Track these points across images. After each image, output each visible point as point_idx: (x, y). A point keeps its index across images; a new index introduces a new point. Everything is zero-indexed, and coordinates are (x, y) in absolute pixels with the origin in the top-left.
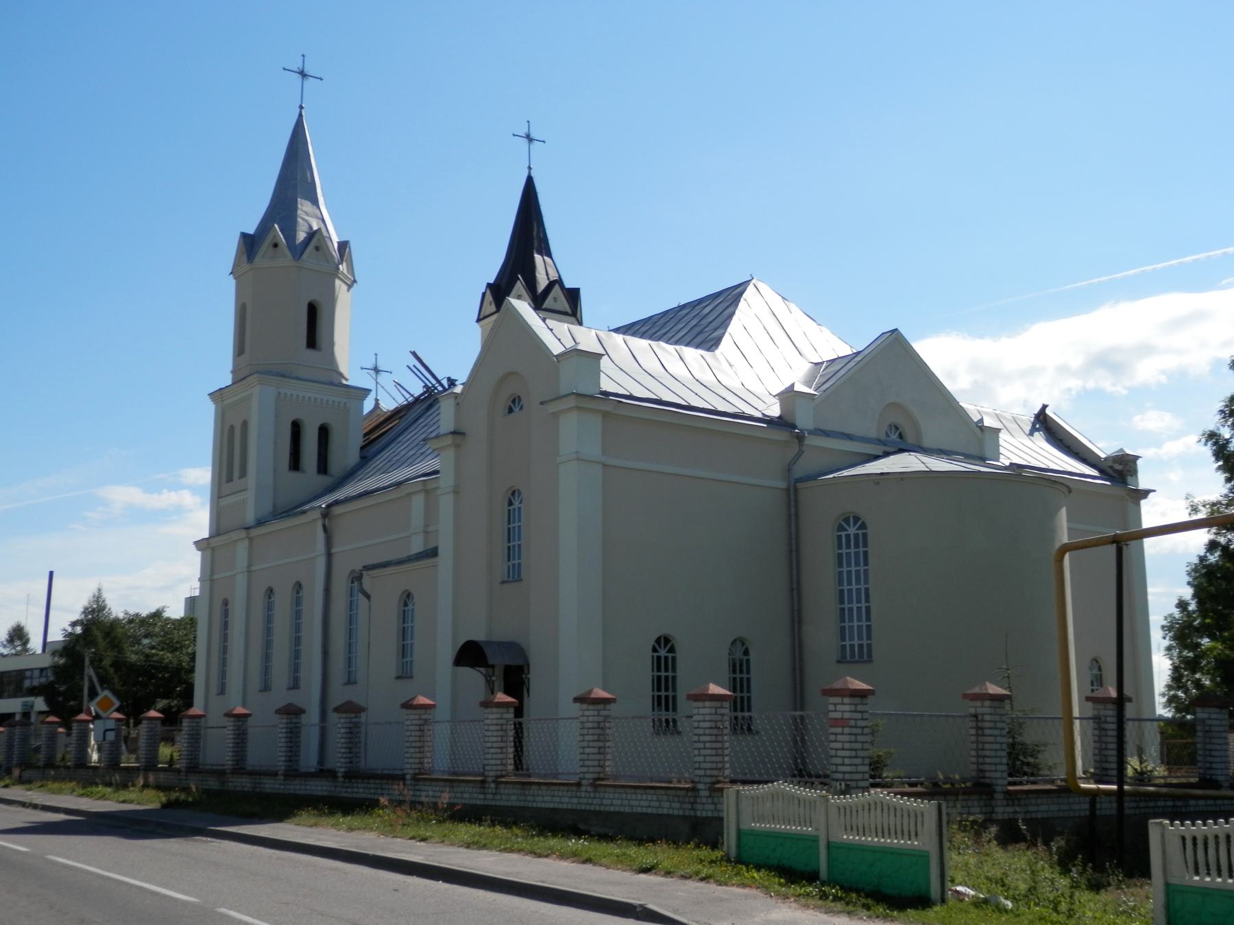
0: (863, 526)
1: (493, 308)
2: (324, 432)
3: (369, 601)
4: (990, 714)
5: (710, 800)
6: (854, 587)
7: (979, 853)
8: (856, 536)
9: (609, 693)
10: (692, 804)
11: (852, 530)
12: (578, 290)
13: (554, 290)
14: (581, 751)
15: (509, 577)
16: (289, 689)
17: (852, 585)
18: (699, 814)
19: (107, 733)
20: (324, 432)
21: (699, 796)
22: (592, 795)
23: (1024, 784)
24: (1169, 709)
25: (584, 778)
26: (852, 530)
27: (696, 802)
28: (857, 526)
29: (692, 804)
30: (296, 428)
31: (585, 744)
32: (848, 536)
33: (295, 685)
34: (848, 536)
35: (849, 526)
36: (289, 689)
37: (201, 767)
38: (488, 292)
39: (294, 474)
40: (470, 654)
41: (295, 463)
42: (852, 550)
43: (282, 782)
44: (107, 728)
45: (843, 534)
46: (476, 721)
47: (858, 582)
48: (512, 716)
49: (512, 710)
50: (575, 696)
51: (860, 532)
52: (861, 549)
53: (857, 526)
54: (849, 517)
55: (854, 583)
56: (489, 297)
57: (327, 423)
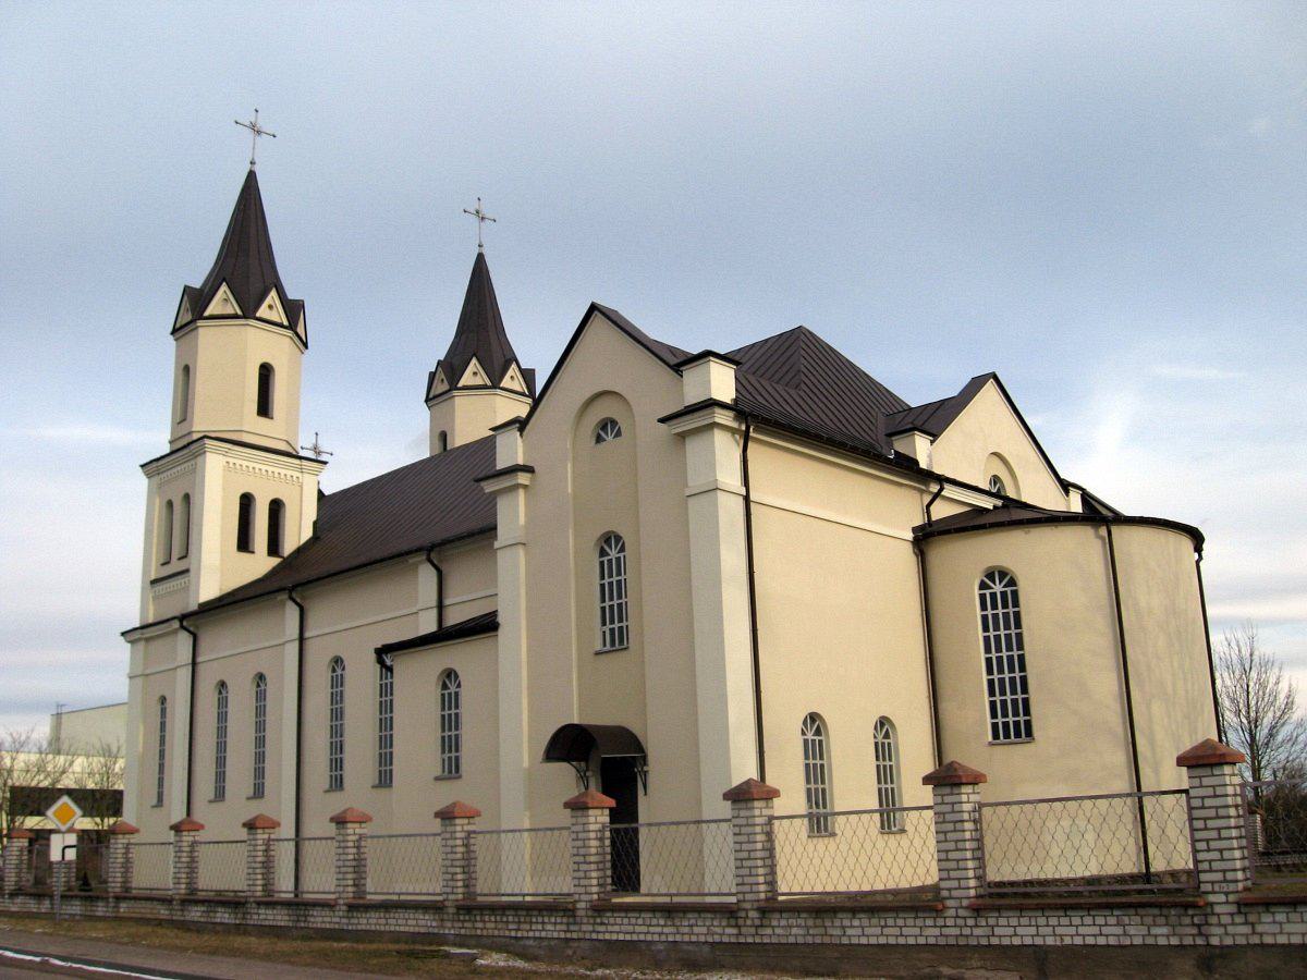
0: (1012, 582)
1: (446, 387)
2: (276, 507)
3: (1198, 549)
4: (348, 847)
5: (1238, 919)
6: (1005, 654)
7: (148, 946)
8: (1004, 594)
9: (636, 792)
10: (1199, 926)
11: (998, 588)
12: (534, 370)
13: (511, 369)
14: (576, 867)
15: (605, 645)
16: (373, 787)
17: (1007, 656)
18: (1215, 941)
19: (67, 850)
20: (276, 507)
21: (1213, 914)
22: (970, 922)
23: (1135, 890)
24: (1298, 801)
25: (340, 898)
26: (998, 588)
27: (1207, 924)
28: (1004, 583)
29: (1199, 926)
30: (247, 502)
31: (341, 863)
32: (993, 595)
33: (259, 792)
34: (993, 595)
35: (1000, 582)
36: (373, 787)
37: (276, 895)
38: (440, 369)
39: (245, 556)
40: (570, 744)
41: (244, 544)
42: (1000, 611)
43: (345, 914)
44: (66, 844)
45: (987, 592)
46: (393, 836)
47: (1009, 648)
48: (607, 819)
49: (607, 812)
50: (243, 821)
51: (1008, 589)
52: (1011, 610)
53: (1004, 583)
54: (993, 573)
55: (1004, 650)
56: (441, 375)
57: (284, 504)
